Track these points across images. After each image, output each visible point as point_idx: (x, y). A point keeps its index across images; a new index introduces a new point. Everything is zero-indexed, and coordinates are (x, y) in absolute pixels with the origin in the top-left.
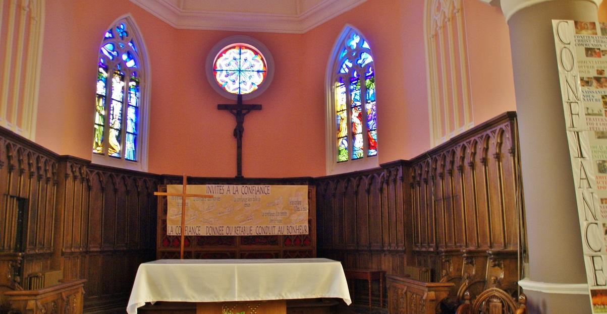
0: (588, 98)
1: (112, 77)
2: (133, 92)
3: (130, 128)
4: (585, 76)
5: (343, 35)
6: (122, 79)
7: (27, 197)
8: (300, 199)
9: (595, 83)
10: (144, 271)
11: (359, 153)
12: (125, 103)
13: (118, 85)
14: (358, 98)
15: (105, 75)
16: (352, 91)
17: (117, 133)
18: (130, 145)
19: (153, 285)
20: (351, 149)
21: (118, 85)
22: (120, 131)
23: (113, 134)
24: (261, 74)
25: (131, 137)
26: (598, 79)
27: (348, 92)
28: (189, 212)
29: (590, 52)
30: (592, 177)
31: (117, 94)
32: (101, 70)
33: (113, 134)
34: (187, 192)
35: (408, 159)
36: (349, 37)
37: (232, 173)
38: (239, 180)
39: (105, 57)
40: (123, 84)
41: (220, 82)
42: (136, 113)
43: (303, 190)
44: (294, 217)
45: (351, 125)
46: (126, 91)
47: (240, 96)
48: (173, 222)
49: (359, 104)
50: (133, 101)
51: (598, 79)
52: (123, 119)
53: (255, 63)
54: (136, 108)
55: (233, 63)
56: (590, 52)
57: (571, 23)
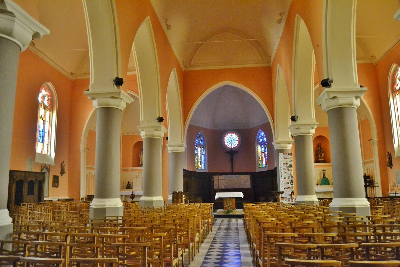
0: (284, 166)
1: (198, 148)
2: (203, 151)
3: (203, 160)
4: (284, 163)
5: (259, 132)
6: (200, 148)
7: (386, 231)
8: (248, 179)
9: (285, 164)
10: (217, 193)
11: (264, 166)
12: (201, 154)
13: (199, 149)
14: (264, 150)
15: (196, 148)
16: (262, 148)
17: (200, 162)
18: (203, 165)
19: (218, 195)
20: (262, 164)
21: (199, 149)
22: (201, 162)
23: (199, 163)
24: (238, 141)
25: (203, 163)
26: (286, 163)
27: (261, 148)
28: (220, 182)
29: (285, 158)
30: (283, 180)
31: (199, 152)
32: (196, 147)
33: (199, 163)
34: (220, 178)
35: (272, 169)
36: (261, 132)
37: (230, 171)
38: (232, 173)
39: (196, 143)
40: (200, 149)
41: (226, 144)
42: (204, 156)
43: (248, 177)
44: (247, 184)
45: (262, 157)
46: (201, 151)
47: (232, 149)
48: (216, 185)
49: (264, 152)
50: (203, 153)
51: (286, 163)
52: (201, 159)
53: (236, 138)
54: (204, 155)
55: (229, 139)
56: (285, 158)
57: (282, 153)
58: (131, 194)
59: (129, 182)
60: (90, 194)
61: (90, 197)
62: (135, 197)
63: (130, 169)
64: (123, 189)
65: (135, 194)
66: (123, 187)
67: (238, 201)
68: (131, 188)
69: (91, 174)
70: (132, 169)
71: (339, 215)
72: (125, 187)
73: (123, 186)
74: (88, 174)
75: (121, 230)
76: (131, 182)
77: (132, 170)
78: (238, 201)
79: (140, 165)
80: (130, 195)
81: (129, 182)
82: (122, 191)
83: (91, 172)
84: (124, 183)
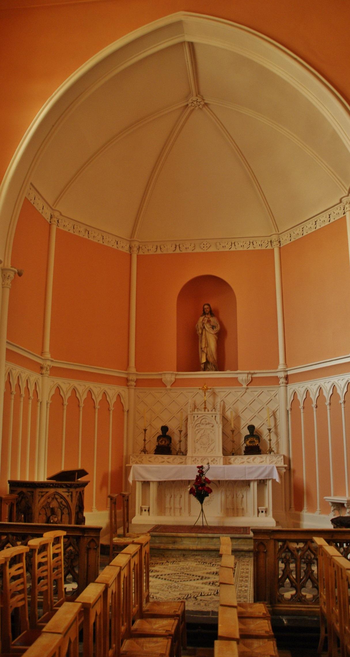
58: (192, 476)
59: (165, 429)
60: (19, 479)
61: (24, 490)
62: (210, 491)
63: (169, 377)
64: (146, 457)
65: (209, 476)
66: (140, 446)
67: (216, 617)
68: (173, 451)
69: (23, 386)
70: (178, 377)
71: (121, 468)
72: (153, 445)
73: (141, 439)
74: (14, 383)
75: (287, 563)
76: (173, 426)
77: (176, 383)
78: (216, 617)
79: (202, 366)
80: (189, 482)
81: (165, 429)
82: (141, 462)
83: (24, 377)
84: (145, 430)
